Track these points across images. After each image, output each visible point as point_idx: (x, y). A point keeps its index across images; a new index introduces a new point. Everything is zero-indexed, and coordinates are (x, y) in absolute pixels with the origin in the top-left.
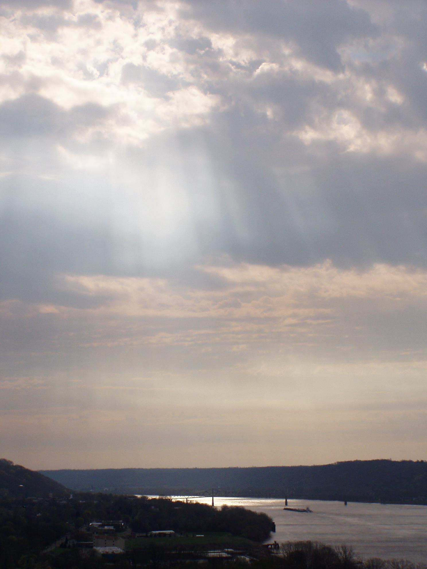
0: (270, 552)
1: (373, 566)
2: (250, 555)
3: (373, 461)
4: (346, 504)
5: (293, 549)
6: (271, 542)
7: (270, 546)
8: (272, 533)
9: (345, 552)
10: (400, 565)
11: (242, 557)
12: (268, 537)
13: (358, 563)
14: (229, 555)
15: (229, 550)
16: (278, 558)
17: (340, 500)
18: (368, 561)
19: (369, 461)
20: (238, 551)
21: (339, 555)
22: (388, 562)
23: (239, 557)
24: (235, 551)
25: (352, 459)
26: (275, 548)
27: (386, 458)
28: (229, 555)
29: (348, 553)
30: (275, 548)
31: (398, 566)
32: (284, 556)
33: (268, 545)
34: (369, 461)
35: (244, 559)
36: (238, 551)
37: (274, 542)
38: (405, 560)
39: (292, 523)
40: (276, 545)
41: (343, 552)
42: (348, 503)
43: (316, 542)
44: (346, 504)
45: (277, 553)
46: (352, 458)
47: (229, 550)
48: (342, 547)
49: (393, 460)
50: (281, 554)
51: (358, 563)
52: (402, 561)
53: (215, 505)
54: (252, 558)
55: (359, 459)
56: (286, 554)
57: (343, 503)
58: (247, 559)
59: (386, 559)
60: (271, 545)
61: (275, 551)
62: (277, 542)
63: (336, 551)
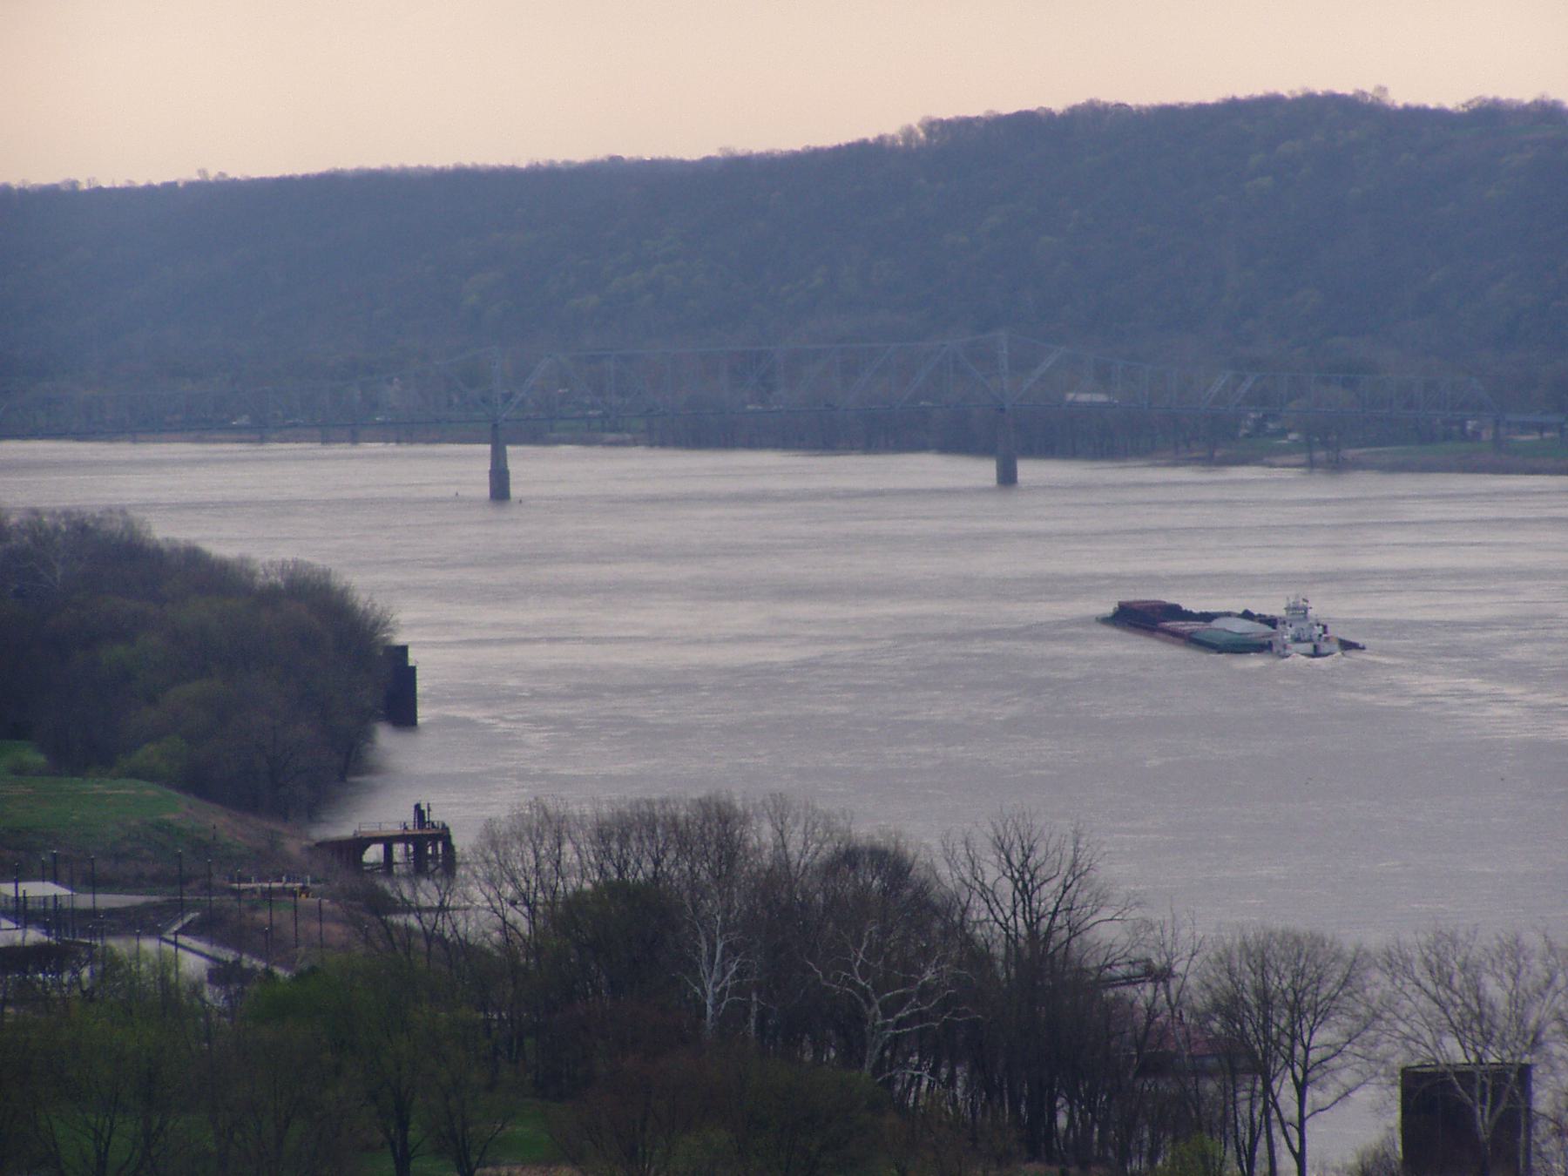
0: (382, 905)
1: (1265, 999)
2: (206, 927)
3: (1233, 109)
4: (1007, 478)
5: (579, 870)
6: (382, 813)
7: (374, 854)
8: (386, 738)
9: (1025, 892)
10: (1495, 991)
11: (149, 945)
12: (348, 765)
13: (1129, 980)
14: (34, 936)
15: (37, 890)
16: (461, 951)
17: (957, 439)
18: (1225, 961)
19: (1201, 112)
20: (106, 900)
21: (978, 911)
22: (1395, 963)
23: (119, 946)
24: (84, 901)
25: (1057, 97)
26: (420, 866)
27: (1345, 87)
28: (34, 936)
29: (1047, 897)
30: (420, 866)
31: (1476, 988)
32: (506, 927)
33: (362, 843)
34: (1201, 110)
35: (165, 967)
36: (106, 900)
37: (409, 817)
38: (1533, 940)
39: (584, 651)
40: (429, 846)
41: (1006, 887)
42: (1029, 470)
43: (779, 811)
44: (1007, 478)
45: (442, 909)
46: (1054, 89)
47: (37, 890)
48: (1001, 846)
49: (1399, 97)
50: (479, 910)
51: (1129, 980)
52: (1515, 950)
53: (487, 448)
54: (229, 955)
55: (1109, 94)
56: (518, 917)
57: (983, 471)
58: (192, 962)
59: (1375, 940)
60: (388, 842)
61: (428, 893)
62: (435, 817)
63: (944, 870)
